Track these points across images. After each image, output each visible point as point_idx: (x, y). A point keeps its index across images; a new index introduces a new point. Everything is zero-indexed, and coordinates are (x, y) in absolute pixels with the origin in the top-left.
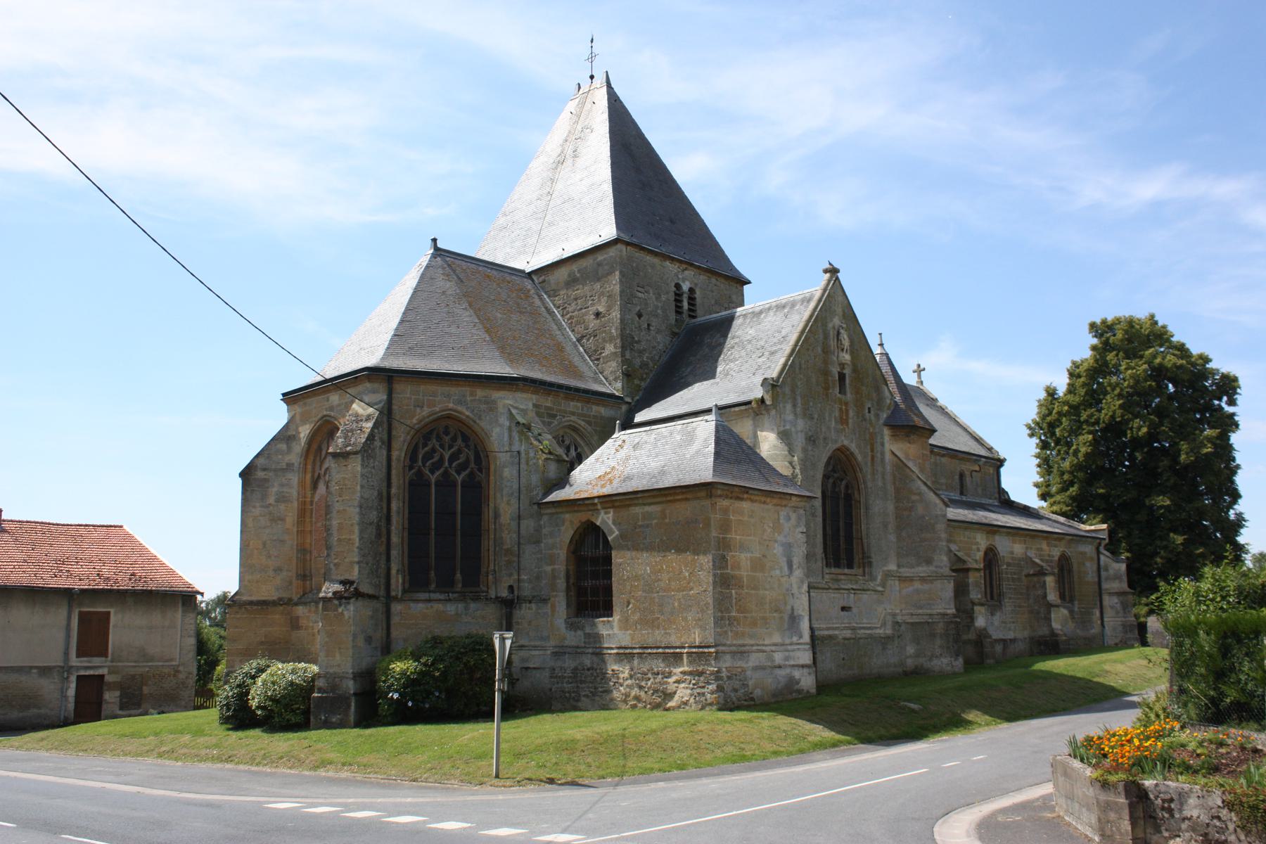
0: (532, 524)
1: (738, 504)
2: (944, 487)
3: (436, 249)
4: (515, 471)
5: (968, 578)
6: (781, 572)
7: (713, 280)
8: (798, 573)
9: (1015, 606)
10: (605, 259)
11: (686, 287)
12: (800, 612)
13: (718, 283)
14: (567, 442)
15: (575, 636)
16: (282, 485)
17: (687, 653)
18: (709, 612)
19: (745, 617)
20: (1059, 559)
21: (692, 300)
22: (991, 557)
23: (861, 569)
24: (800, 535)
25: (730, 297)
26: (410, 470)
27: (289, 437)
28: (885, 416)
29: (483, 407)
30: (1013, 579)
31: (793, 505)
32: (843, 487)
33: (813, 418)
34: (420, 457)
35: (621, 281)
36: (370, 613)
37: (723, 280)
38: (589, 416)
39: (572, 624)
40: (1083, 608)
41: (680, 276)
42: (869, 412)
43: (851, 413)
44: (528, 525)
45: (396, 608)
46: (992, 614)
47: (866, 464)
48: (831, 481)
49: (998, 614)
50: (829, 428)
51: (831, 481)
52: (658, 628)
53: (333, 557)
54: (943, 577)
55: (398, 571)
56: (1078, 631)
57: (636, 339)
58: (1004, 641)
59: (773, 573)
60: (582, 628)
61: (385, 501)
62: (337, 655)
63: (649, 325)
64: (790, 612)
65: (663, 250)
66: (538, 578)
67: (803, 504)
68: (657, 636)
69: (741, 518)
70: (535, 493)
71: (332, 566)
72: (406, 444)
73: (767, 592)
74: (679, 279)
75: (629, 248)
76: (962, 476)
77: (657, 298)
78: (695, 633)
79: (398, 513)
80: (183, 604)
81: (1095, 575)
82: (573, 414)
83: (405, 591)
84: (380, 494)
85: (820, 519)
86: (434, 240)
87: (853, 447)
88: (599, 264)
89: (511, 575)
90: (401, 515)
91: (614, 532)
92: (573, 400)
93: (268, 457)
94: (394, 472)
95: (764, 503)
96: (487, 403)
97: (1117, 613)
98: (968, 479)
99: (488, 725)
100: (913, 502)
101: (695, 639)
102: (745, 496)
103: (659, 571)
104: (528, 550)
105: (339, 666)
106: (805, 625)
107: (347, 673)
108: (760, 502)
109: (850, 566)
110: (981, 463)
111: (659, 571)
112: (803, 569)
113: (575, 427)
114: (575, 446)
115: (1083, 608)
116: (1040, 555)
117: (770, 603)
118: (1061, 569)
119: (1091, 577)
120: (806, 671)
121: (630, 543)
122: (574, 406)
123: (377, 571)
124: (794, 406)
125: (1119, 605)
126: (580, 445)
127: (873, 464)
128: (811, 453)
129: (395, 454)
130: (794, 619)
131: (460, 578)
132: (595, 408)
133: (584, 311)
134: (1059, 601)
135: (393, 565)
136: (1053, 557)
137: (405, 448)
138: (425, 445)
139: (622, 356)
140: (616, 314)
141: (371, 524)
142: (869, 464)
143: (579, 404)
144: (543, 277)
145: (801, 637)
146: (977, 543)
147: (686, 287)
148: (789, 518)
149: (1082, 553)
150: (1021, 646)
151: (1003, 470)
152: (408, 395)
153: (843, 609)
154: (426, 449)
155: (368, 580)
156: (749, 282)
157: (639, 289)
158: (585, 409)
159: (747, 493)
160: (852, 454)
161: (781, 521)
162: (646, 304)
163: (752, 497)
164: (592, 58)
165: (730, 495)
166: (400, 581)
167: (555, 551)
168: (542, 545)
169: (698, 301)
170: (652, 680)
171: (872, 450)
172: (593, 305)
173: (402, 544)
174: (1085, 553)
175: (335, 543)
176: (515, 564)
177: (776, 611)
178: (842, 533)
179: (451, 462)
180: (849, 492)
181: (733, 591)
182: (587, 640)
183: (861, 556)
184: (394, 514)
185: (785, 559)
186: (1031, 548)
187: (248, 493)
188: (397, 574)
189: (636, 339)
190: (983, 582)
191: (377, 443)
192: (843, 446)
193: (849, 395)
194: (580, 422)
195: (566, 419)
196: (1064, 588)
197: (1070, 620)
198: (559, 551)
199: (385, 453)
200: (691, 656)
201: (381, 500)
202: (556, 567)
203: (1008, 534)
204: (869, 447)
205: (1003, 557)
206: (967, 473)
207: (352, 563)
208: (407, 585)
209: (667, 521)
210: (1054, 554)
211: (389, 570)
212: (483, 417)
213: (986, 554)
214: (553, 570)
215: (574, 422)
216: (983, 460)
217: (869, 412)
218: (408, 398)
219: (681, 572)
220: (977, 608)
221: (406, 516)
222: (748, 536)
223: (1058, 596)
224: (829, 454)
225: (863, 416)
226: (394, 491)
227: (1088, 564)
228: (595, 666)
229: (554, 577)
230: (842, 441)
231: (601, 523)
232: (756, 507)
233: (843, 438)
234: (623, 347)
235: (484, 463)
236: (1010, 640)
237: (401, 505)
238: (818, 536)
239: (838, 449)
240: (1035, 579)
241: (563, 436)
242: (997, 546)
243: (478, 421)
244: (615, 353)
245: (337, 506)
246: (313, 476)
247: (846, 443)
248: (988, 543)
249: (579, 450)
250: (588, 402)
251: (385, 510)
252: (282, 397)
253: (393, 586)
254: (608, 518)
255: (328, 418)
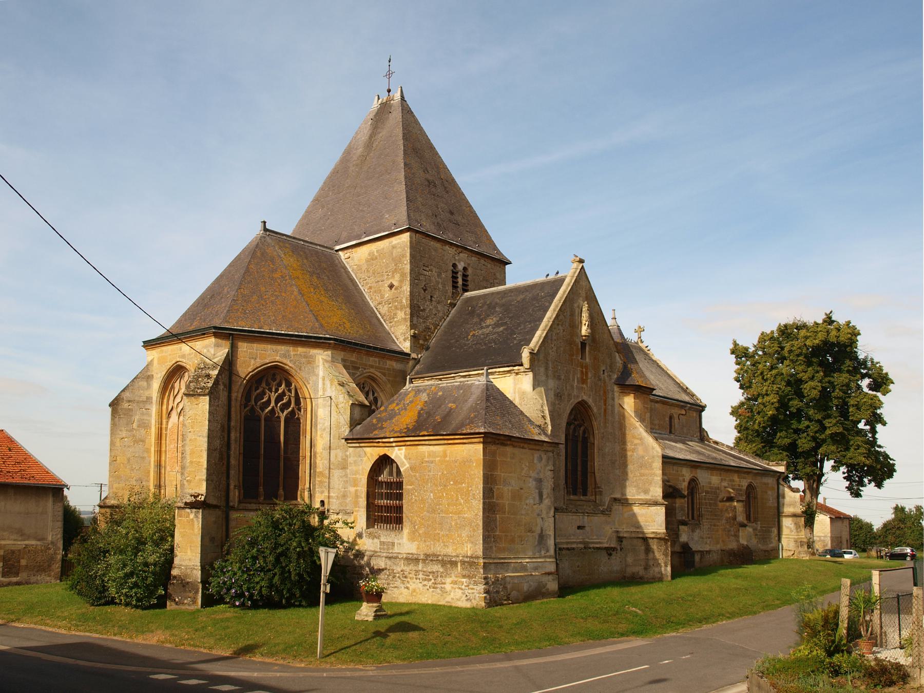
0: (341, 454)
1: (502, 448)
2: (657, 427)
3: (266, 230)
4: (327, 412)
5: (675, 503)
6: (534, 501)
7: (482, 261)
8: (547, 502)
9: (711, 525)
10: (398, 244)
11: (460, 266)
12: (548, 533)
13: (486, 264)
14: (366, 389)
15: (372, 543)
16: (143, 414)
17: (461, 562)
18: (479, 531)
19: (506, 536)
20: (747, 488)
21: (465, 276)
22: (693, 482)
23: (594, 497)
24: (549, 472)
25: (495, 275)
26: (245, 408)
27: (149, 376)
28: (616, 376)
29: (303, 360)
30: (710, 504)
31: (544, 449)
32: (581, 432)
33: (560, 379)
34: (254, 397)
35: (410, 262)
36: (214, 519)
37: (490, 261)
38: (385, 369)
39: (370, 534)
40: (764, 527)
41: (457, 258)
42: (603, 374)
43: (590, 375)
44: (337, 455)
45: (234, 515)
46: (693, 531)
47: (600, 414)
48: (572, 427)
49: (698, 531)
50: (572, 387)
51: (572, 427)
52: (439, 541)
53: (186, 475)
54: (656, 504)
55: (235, 486)
56: (760, 545)
57: (422, 308)
58: (702, 552)
59: (528, 501)
60: (378, 537)
61: (226, 431)
62: (189, 552)
63: (431, 297)
64: (539, 532)
65: (444, 237)
66: (344, 496)
67: (551, 449)
68: (439, 548)
69: (505, 459)
70: (343, 429)
71: (185, 482)
72: (242, 388)
73: (523, 517)
74: (455, 260)
75: (417, 235)
76: (671, 418)
77: (438, 276)
78: (467, 547)
79: (236, 441)
80: (53, 496)
81: (775, 501)
82: (372, 367)
83: (240, 502)
84: (222, 426)
85: (563, 458)
86: (265, 222)
87: (590, 401)
88: (394, 247)
89: (322, 492)
90: (238, 443)
91: (405, 465)
92: (372, 356)
93: (132, 392)
94: (233, 409)
95: (523, 448)
96: (305, 357)
97: (791, 531)
98: (676, 421)
99: (311, 611)
100: (636, 445)
101: (467, 551)
102: (509, 443)
103: (440, 497)
104: (336, 473)
105: (190, 560)
106: (551, 543)
107: (196, 566)
108: (520, 447)
109: (585, 494)
110: (687, 408)
111: (440, 497)
112: (550, 498)
113: (373, 377)
114: (373, 391)
115: (764, 527)
116: (732, 485)
117: (525, 525)
118: (748, 496)
119: (772, 502)
120: (551, 577)
121: (417, 474)
122: (372, 360)
123: (219, 486)
124: (547, 369)
125: (793, 525)
126: (376, 390)
127: (605, 415)
128: (557, 406)
129: (234, 395)
130: (542, 537)
131: (283, 493)
132: (388, 362)
133: (380, 283)
134: (745, 522)
135: (231, 481)
136: (742, 486)
137: (242, 390)
138: (257, 389)
139: (411, 322)
140: (407, 288)
141: (215, 450)
142: (602, 414)
143: (377, 359)
144: (348, 254)
145: (548, 551)
146: (683, 475)
147: (460, 266)
148: (540, 459)
149: (765, 484)
150: (715, 557)
151: (703, 414)
152: (245, 349)
153: (579, 528)
154: (258, 391)
155: (213, 494)
156: (510, 263)
157: (424, 268)
158: (381, 363)
159: (510, 440)
160: (589, 406)
161: (535, 462)
162: (430, 280)
163: (514, 443)
164: (389, 75)
165: (497, 442)
166: (237, 494)
167: (357, 476)
168: (348, 471)
169: (469, 278)
170: (433, 581)
171: (605, 405)
172: (388, 279)
173: (239, 465)
174: (768, 484)
175: (188, 465)
176: (326, 484)
177: (529, 531)
178: (579, 468)
179: (277, 402)
180: (586, 436)
181: (498, 516)
182: (382, 547)
183: (593, 486)
184: (232, 442)
185: (537, 491)
186: (725, 480)
187: (117, 419)
188: (235, 488)
189: (422, 308)
190: (686, 506)
191: (221, 387)
192: (583, 400)
193: (587, 360)
194: (377, 373)
195: (367, 370)
196: (750, 511)
197: (753, 536)
198: (361, 477)
199: (226, 394)
200: (464, 564)
201: (223, 431)
202: (359, 488)
203: (708, 468)
204: (602, 401)
205: (703, 486)
206: (676, 416)
207: (201, 480)
208: (242, 497)
209: (447, 459)
210: (743, 484)
211: (228, 485)
212: (303, 368)
213: (689, 483)
214: (356, 491)
215: (372, 373)
216: (689, 405)
217: (603, 374)
218: (245, 352)
219: (457, 499)
220: (682, 528)
221: (242, 444)
222: (510, 473)
223: (745, 518)
224: (571, 408)
225: (599, 376)
226: (232, 424)
227: (770, 493)
228: (388, 568)
229: (357, 496)
230: (582, 396)
231: (396, 457)
232: (517, 451)
233: (583, 394)
234: (412, 315)
235: (302, 404)
236: (706, 551)
237: (238, 435)
238: (562, 471)
239: (579, 403)
240: (728, 504)
241: (363, 384)
242: (698, 478)
243: (298, 371)
244: (405, 318)
245: (190, 436)
246: (167, 408)
247: (585, 398)
248: (692, 475)
249: (376, 395)
250: (383, 358)
251: (226, 439)
252: (143, 344)
253: (231, 498)
254: (401, 454)
255: (180, 363)
